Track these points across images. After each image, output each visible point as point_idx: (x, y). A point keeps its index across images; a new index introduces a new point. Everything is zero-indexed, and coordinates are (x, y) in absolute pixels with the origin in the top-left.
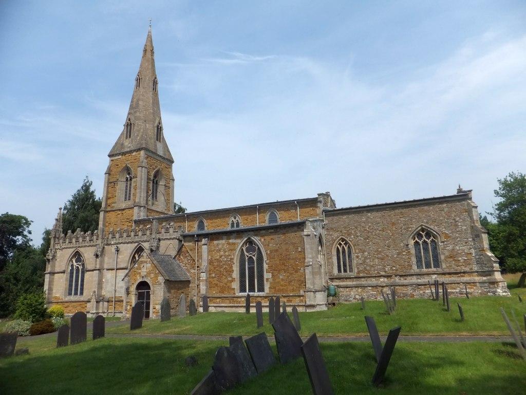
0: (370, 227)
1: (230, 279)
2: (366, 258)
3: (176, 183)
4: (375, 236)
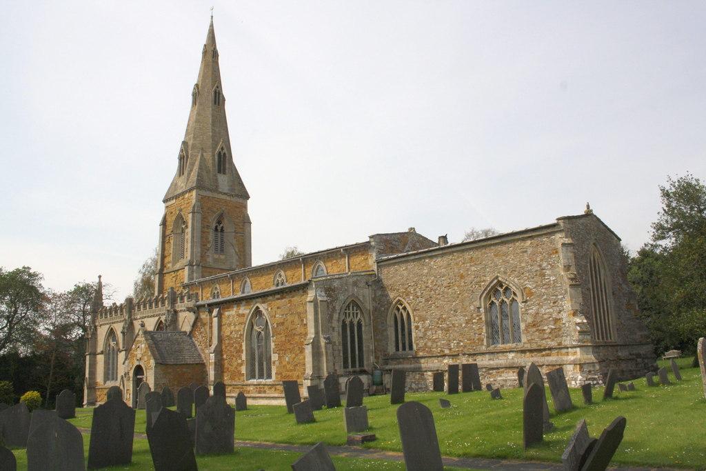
0: (433, 282)
1: (240, 361)
2: (427, 329)
3: (253, 226)
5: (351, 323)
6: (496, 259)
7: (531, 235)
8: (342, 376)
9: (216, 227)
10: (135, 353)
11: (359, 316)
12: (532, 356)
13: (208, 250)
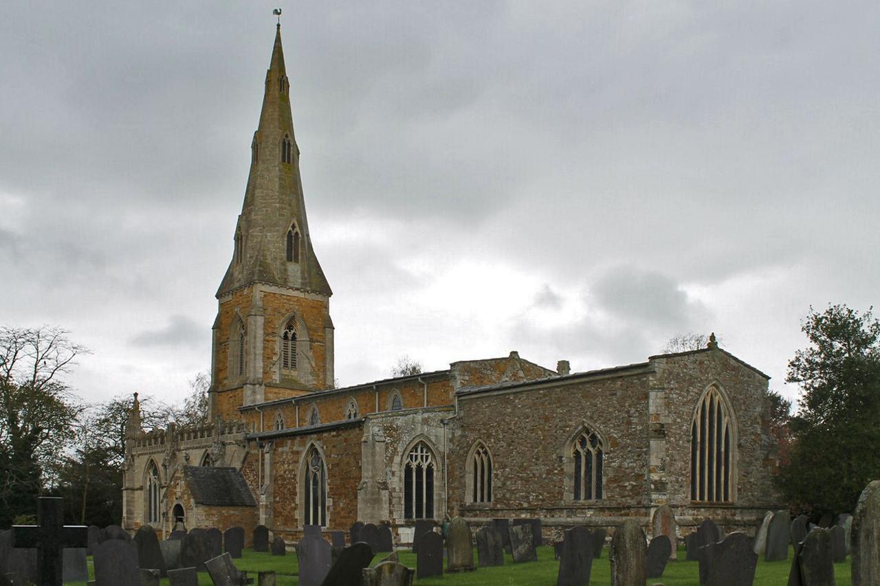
1: (293, 505)
2: (507, 478)
4: (520, 441)
5: (419, 468)
6: (583, 401)
7: (620, 375)
8: (402, 526)
9: (286, 333)
10: (175, 490)
11: (429, 460)
12: (610, 515)
13: (274, 364)
